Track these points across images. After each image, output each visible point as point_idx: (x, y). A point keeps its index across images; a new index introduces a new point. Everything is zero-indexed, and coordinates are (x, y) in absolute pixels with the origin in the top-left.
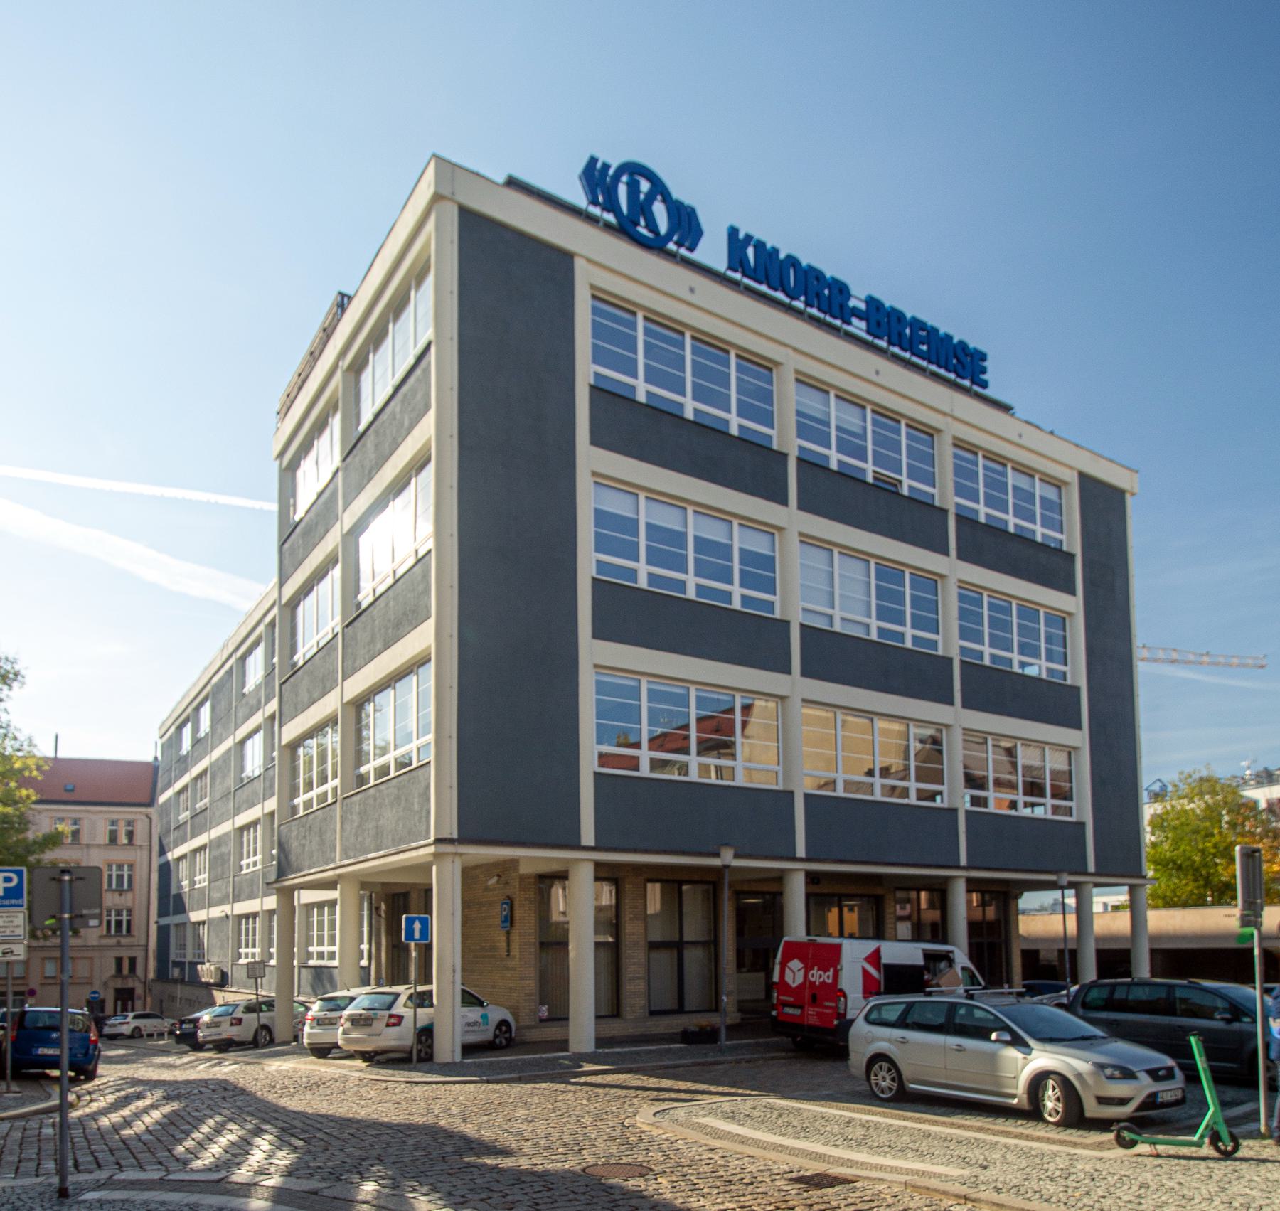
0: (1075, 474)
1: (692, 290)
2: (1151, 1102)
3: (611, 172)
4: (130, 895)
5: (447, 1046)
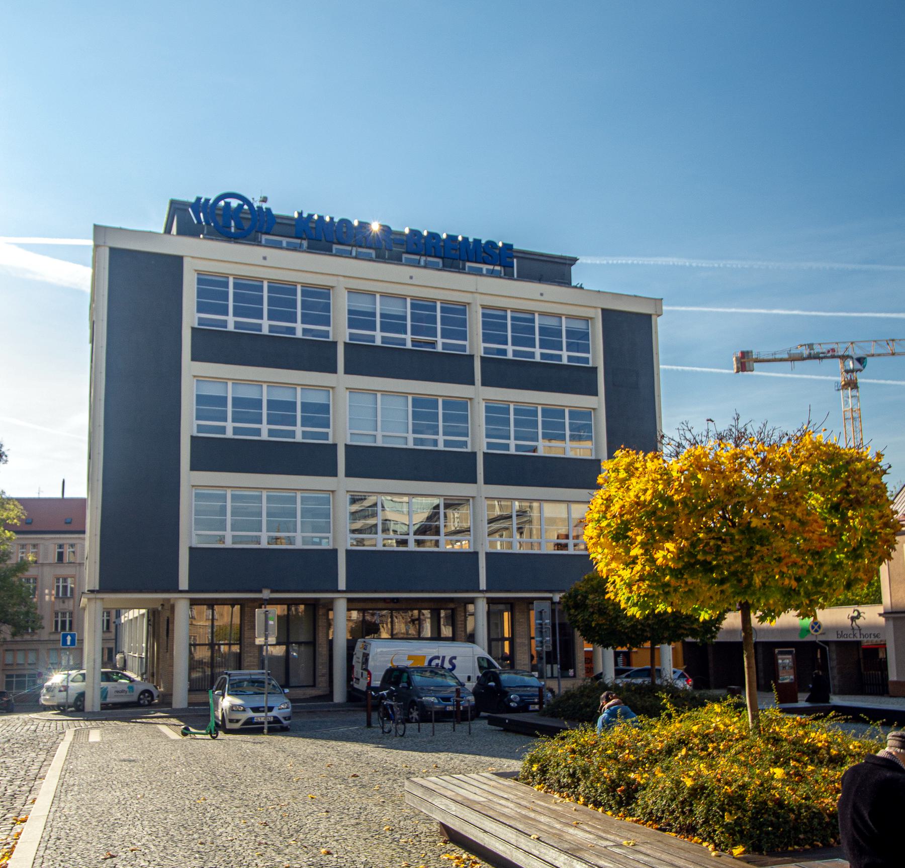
0: (600, 311)
1: (265, 258)
2: (250, 721)
3: (211, 202)
4: (71, 602)
5: (92, 703)
